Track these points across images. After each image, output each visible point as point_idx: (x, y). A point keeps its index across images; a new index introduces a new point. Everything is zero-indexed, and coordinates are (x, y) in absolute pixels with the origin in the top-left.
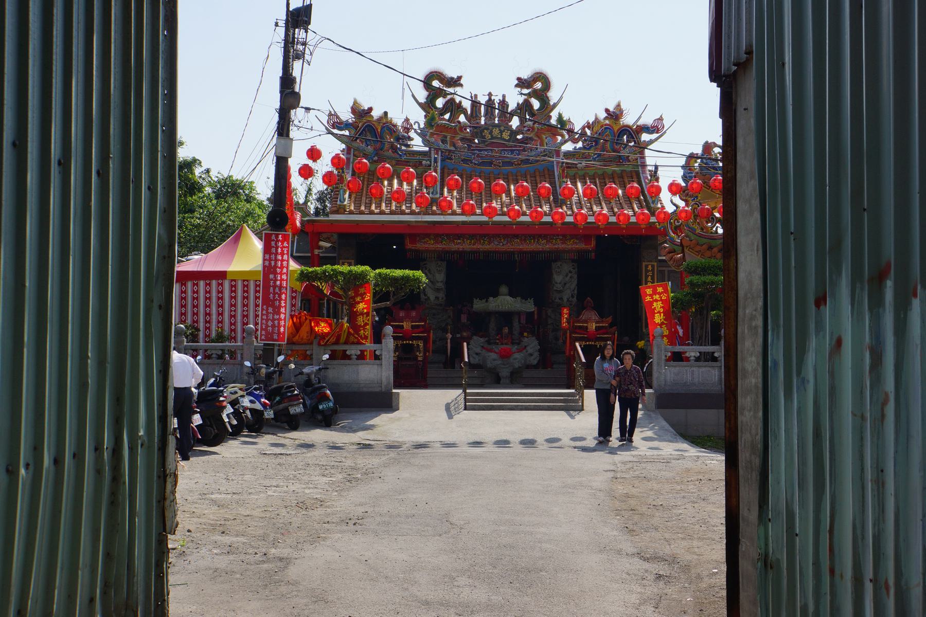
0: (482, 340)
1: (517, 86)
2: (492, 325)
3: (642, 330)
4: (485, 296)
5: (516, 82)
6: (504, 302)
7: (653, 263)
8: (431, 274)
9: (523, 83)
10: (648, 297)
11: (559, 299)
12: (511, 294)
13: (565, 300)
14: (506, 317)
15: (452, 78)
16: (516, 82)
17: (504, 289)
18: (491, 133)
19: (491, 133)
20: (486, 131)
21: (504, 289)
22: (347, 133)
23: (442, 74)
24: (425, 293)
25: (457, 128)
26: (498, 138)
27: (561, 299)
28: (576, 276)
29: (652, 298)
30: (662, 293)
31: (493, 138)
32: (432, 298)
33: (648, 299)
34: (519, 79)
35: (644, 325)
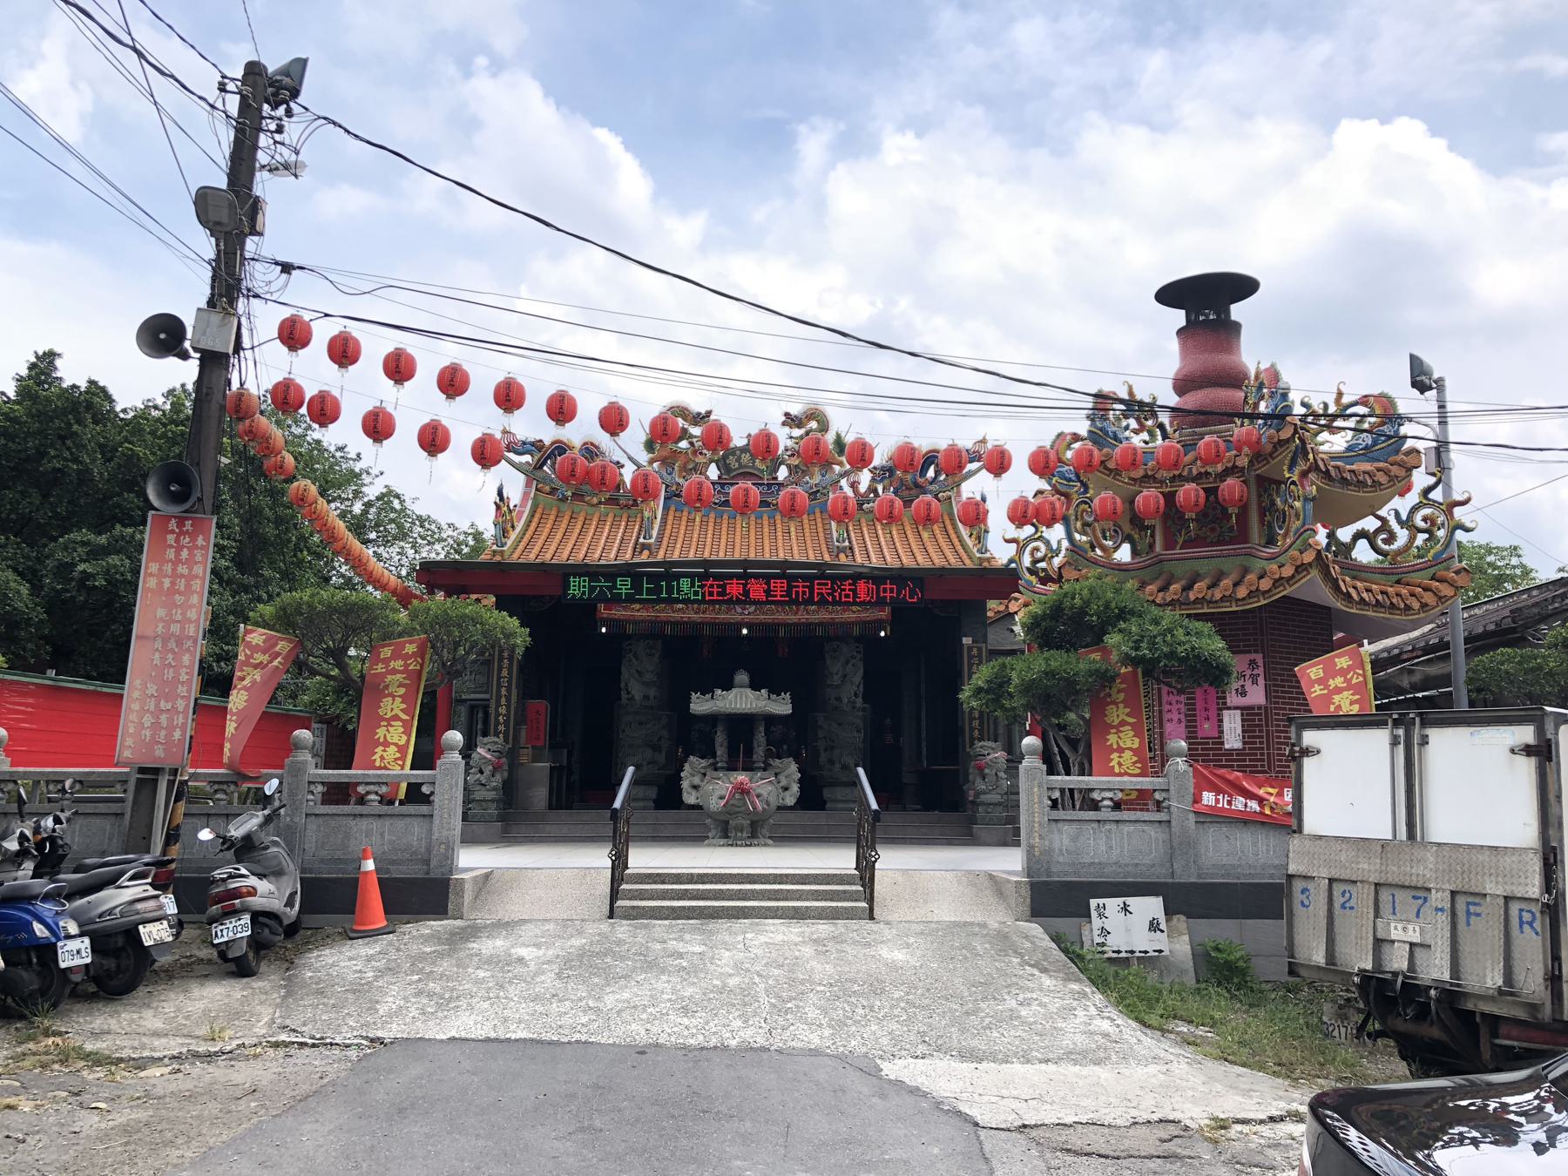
0: (704, 763)
1: (784, 424)
2: (720, 739)
3: (964, 747)
4: (707, 690)
5: (784, 418)
6: (741, 699)
7: (979, 645)
8: (637, 659)
9: (792, 420)
10: (1317, 687)
11: (836, 699)
12: (755, 686)
13: (845, 700)
14: (741, 726)
15: (699, 414)
16: (784, 418)
17: (742, 677)
18: (738, 460)
19: (738, 460)
20: (731, 457)
21: (742, 677)
22: (527, 458)
23: (686, 409)
24: (627, 690)
25: (689, 451)
26: (749, 467)
27: (839, 699)
28: (861, 665)
29: (1327, 687)
30: (1350, 668)
31: (741, 466)
32: (638, 696)
33: (1317, 690)
34: (787, 415)
35: (967, 740)
